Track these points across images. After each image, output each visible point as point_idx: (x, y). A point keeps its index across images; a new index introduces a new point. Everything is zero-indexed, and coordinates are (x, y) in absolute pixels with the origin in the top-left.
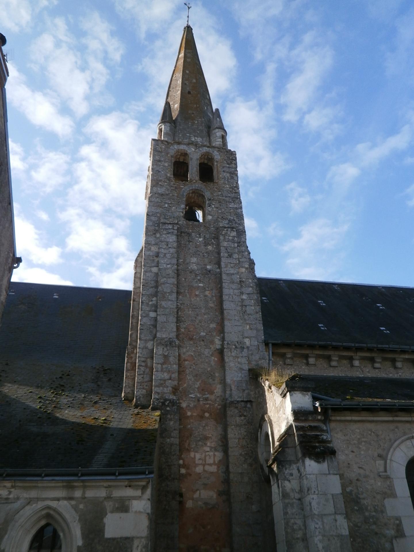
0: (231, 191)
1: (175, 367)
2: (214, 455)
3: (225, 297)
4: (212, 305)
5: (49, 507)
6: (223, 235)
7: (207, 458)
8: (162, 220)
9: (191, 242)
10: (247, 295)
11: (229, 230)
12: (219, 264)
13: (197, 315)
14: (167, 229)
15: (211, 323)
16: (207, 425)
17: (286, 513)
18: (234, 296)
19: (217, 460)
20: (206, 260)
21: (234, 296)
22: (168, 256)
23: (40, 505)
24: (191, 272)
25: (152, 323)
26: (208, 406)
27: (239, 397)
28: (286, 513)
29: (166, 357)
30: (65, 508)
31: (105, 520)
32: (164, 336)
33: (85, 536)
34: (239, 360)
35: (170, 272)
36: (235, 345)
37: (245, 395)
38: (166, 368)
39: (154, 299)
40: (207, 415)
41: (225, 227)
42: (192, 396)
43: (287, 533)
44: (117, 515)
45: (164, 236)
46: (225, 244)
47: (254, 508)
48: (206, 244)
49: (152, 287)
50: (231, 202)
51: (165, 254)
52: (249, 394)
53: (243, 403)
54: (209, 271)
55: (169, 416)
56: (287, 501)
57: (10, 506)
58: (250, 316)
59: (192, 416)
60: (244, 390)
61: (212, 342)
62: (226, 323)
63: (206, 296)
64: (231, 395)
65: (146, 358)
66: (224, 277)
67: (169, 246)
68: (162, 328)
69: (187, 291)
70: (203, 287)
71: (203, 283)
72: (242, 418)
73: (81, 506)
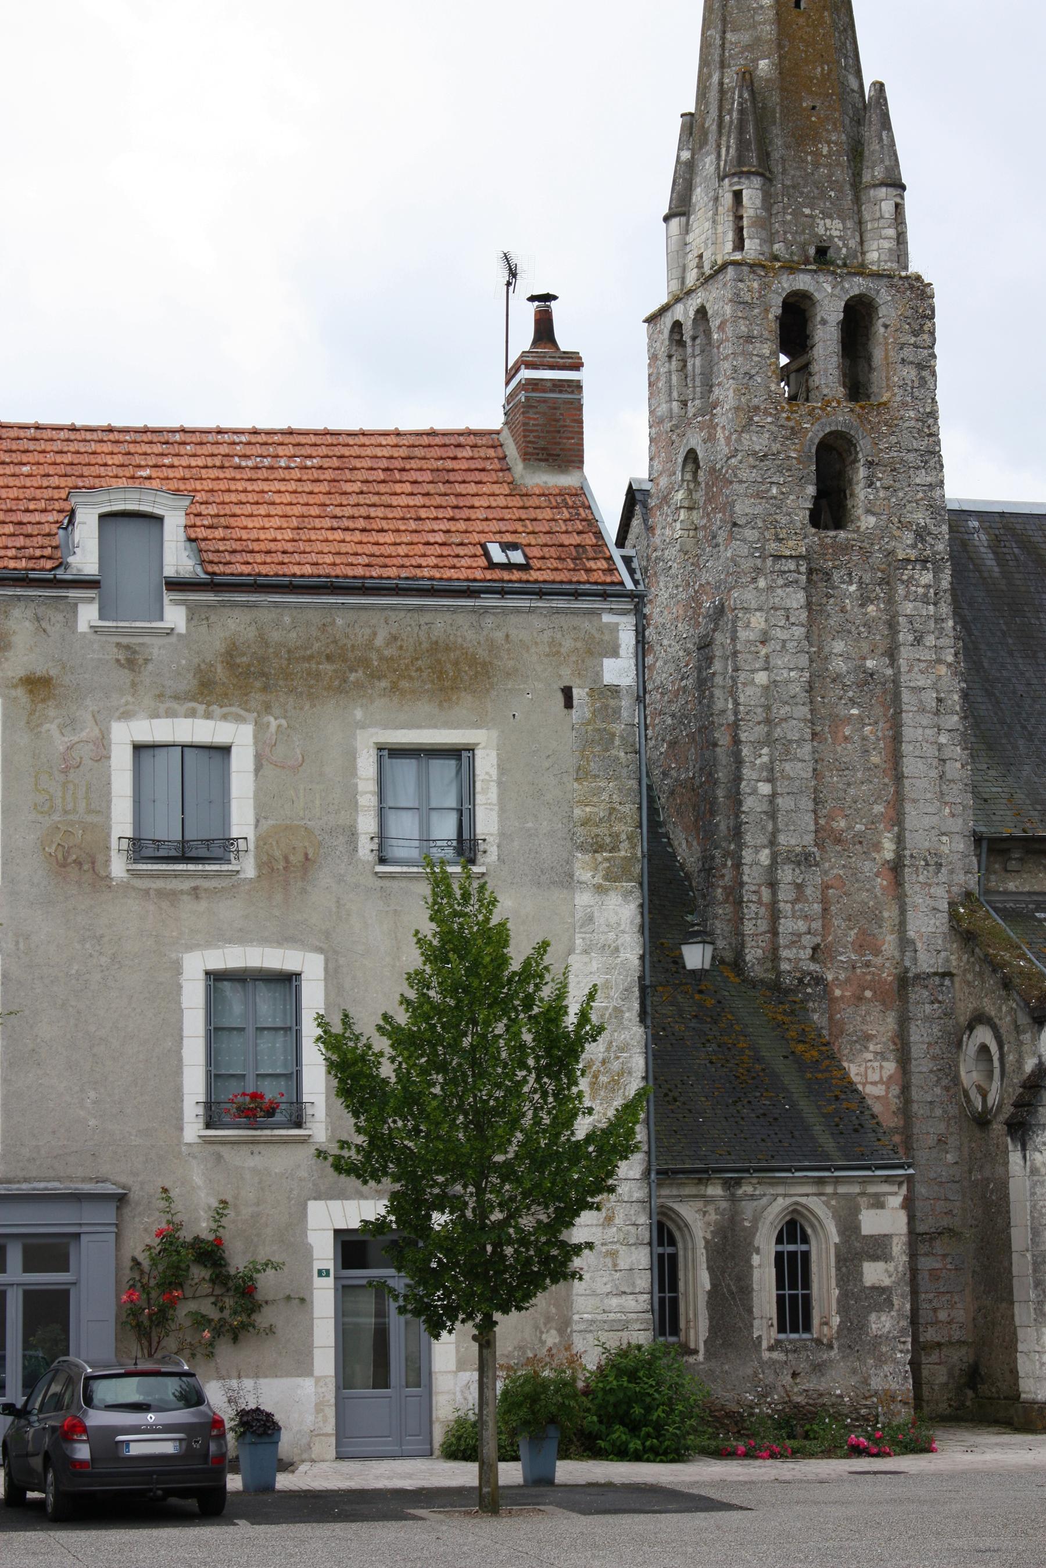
0: (920, 431)
1: (817, 907)
2: (881, 1067)
3: (906, 748)
4: (875, 759)
5: (796, 1203)
6: (903, 582)
7: (870, 1071)
8: (773, 547)
9: (832, 596)
10: (947, 734)
11: (918, 567)
12: (892, 654)
13: (849, 784)
14: (785, 572)
15: (875, 802)
16: (868, 1013)
17: (1033, 1194)
18: (924, 744)
19: (886, 1074)
20: (865, 646)
21: (924, 744)
22: (790, 645)
23: (789, 1201)
24: (834, 681)
25: (765, 807)
26: (869, 977)
27: (930, 966)
28: (1033, 1194)
29: (799, 887)
30: (816, 1204)
31: (861, 1217)
32: (793, 842)
33: (841, 1233)
34: (932, 890)
35: (796, 689)
36: (925, 860)
37: (940, 961)
38: (801, 910)
39: (765, 751)
40: (868, 994)
41: (908, 560)
42: (842, 958)
43: (1033, 1218)
44: (872, 1212)
45: (779, 591)
46: (908, 608)
47: (950, 1158)
48: (865, 601)
49: (759, 723)
50: (918, 468)
51: (784, 641)
52: (947, 960)
53: (937, 979)
54: (872, 675)
55: (811, 1004)
56: (1035, 1178)
57: (755, 1203)
58: (952, 785)
59: (842, 997)
60: (939, 952)
61: (877, 846)
62: (908, 807)
63: (864, 739)
64: (915, 960)
65: (760, 885)
66: (906, 696)
67: (792, 620)
68: (787, 825)
69: (827, 729)
70: (859, 716)
71: (860, 706)
72: (936, 1006)
73: (833, 1202)
